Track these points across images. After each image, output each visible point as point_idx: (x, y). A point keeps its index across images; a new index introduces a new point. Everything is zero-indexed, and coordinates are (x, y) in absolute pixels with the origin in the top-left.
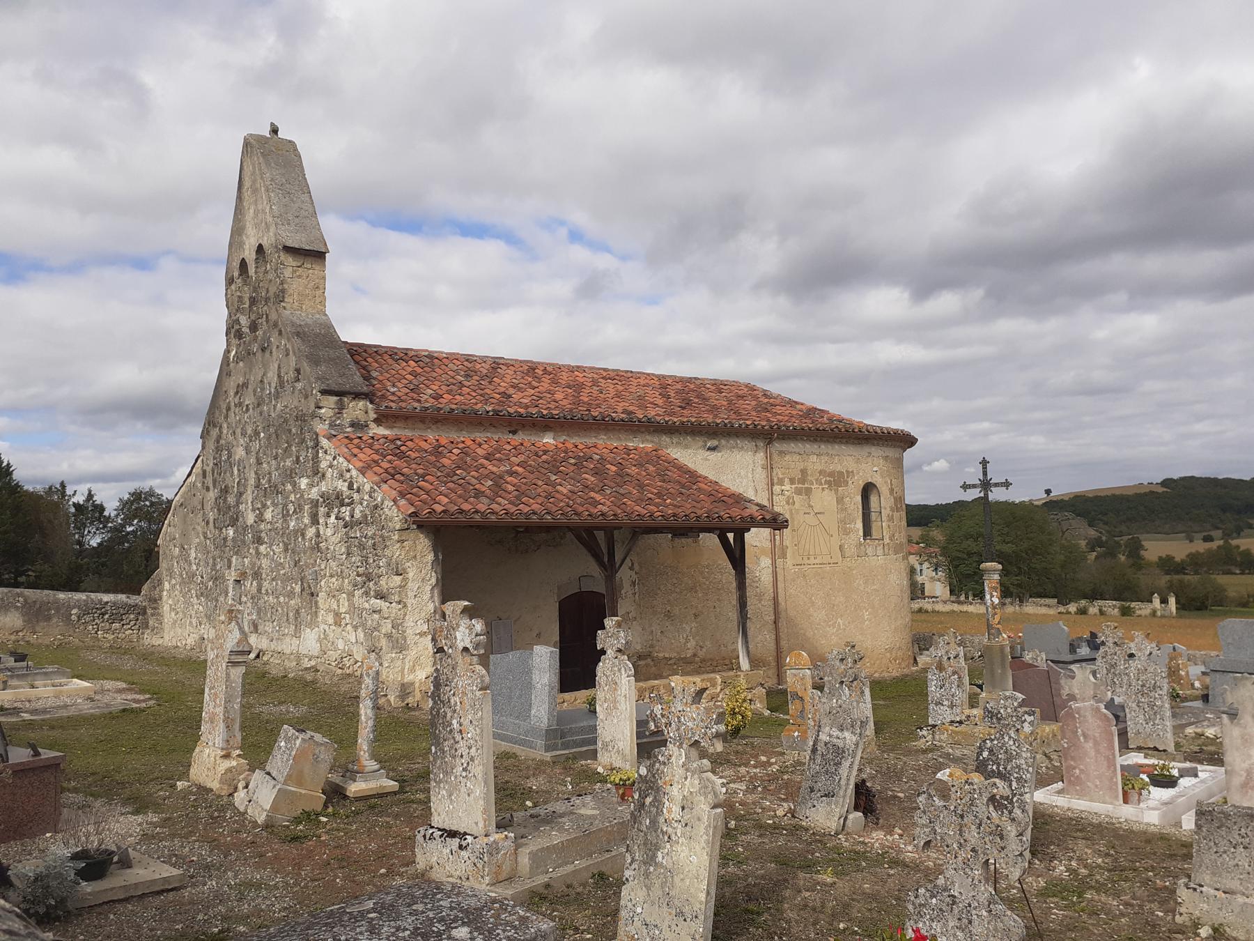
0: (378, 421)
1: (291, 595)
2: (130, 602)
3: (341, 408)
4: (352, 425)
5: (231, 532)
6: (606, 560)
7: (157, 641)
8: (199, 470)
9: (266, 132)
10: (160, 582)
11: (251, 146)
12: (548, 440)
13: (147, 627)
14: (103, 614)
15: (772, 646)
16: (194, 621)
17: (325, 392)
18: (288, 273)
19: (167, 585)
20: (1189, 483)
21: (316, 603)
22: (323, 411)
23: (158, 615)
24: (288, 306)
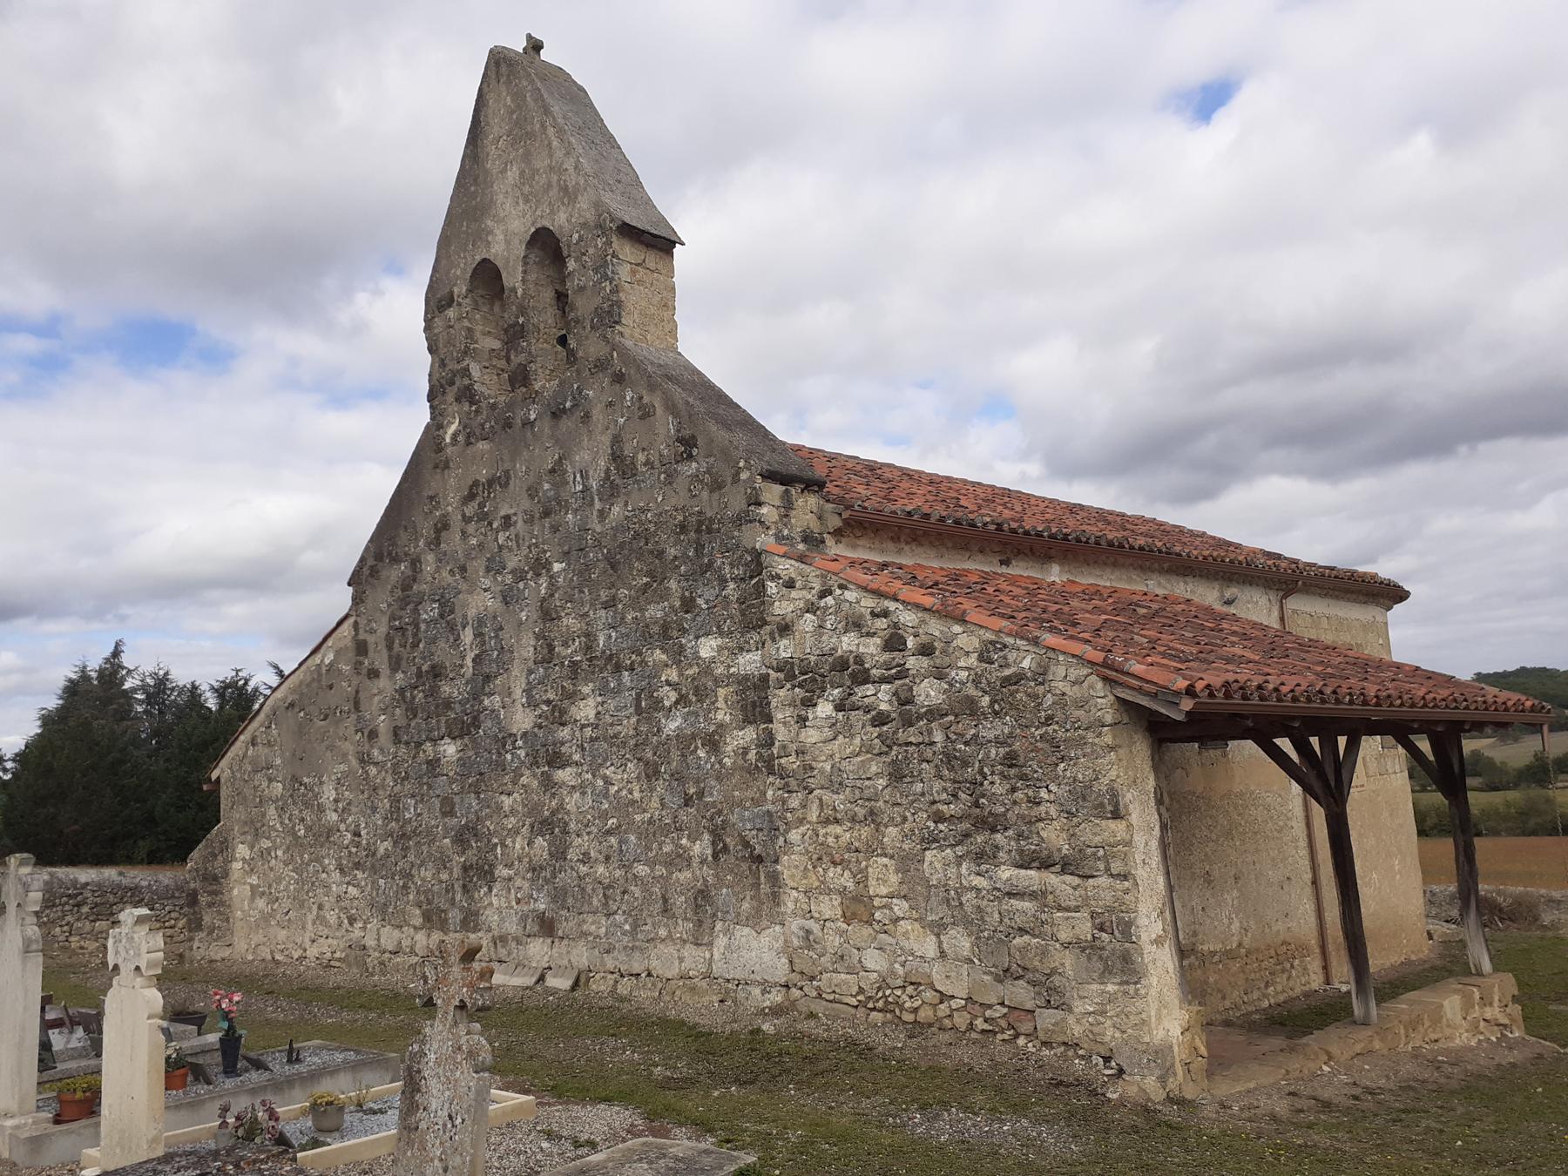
0: (838, 534)
1: (680, 859)
2: (125, 882)
3: (788, 505)
4: (805, 540)
5: (450, 749)
6: (1333, 784)
7: (218, 952)
8: (348, 642)
9: (519, 45)
10: (226, 845)
11: (499, 62)
12: (1055, 574)
13: (199, 927)
14: (78, 905)
15: (1312, 920)
16: (332, 917)
17: (771, 476)
18: (624, 272)
19: (242, 851)
20: (1544, 670)
21: (774, 878)
22: (764, 510)
23: (221, 904)
24: (627, 332)
